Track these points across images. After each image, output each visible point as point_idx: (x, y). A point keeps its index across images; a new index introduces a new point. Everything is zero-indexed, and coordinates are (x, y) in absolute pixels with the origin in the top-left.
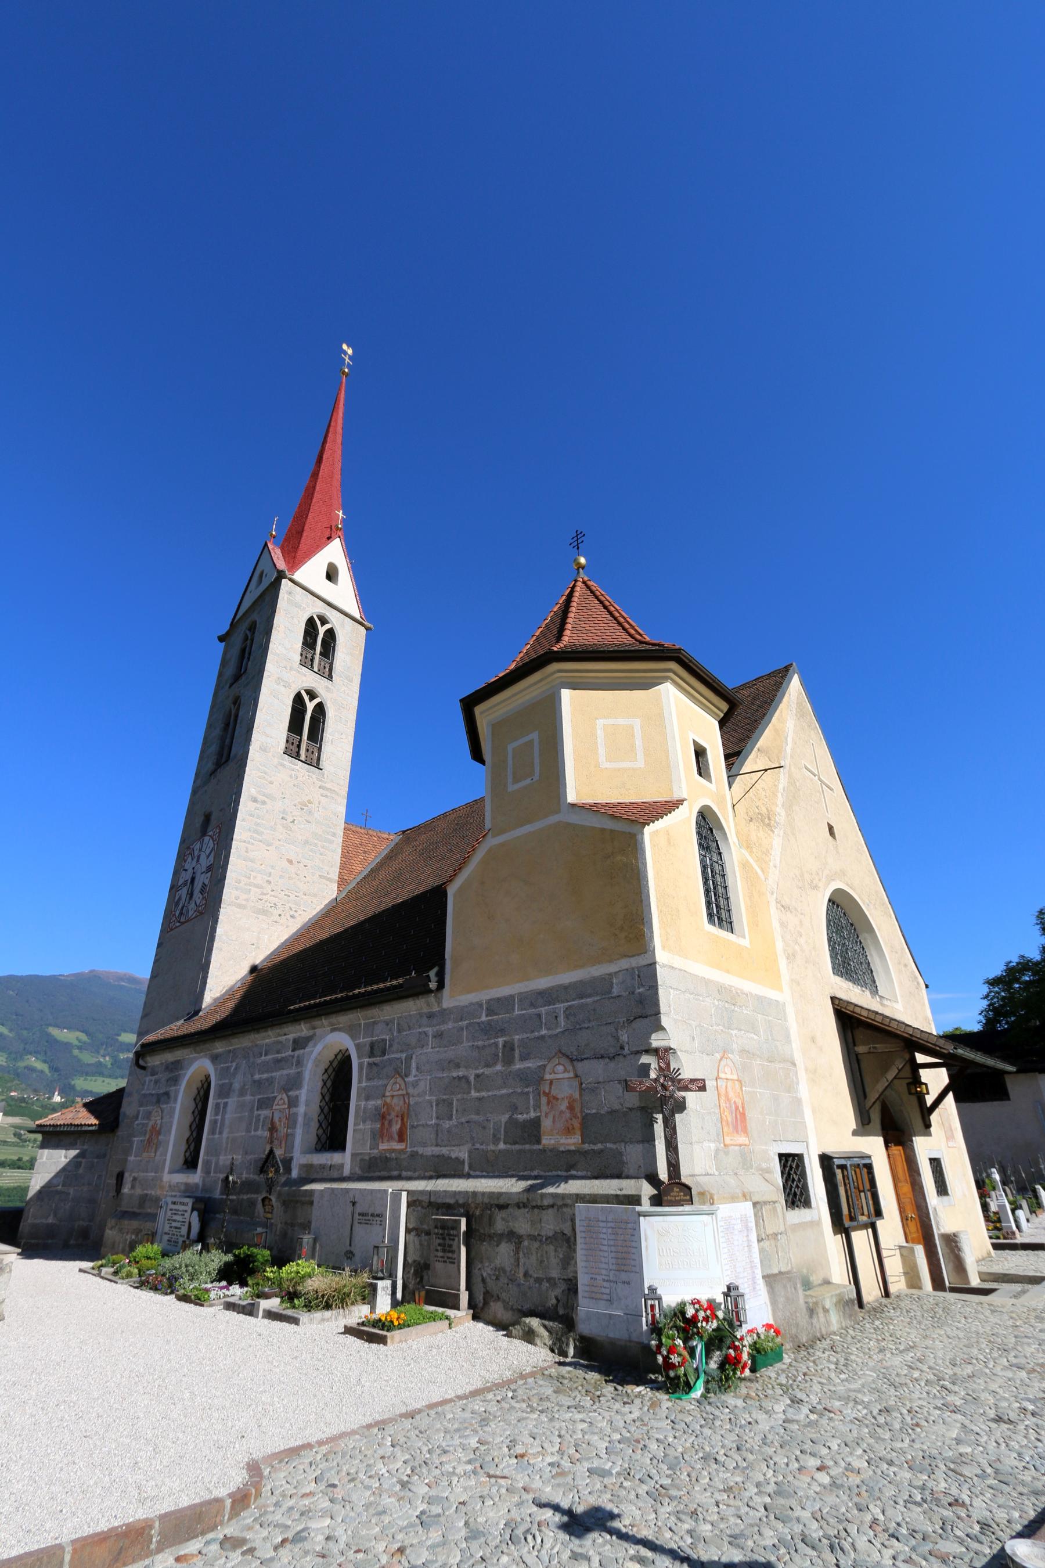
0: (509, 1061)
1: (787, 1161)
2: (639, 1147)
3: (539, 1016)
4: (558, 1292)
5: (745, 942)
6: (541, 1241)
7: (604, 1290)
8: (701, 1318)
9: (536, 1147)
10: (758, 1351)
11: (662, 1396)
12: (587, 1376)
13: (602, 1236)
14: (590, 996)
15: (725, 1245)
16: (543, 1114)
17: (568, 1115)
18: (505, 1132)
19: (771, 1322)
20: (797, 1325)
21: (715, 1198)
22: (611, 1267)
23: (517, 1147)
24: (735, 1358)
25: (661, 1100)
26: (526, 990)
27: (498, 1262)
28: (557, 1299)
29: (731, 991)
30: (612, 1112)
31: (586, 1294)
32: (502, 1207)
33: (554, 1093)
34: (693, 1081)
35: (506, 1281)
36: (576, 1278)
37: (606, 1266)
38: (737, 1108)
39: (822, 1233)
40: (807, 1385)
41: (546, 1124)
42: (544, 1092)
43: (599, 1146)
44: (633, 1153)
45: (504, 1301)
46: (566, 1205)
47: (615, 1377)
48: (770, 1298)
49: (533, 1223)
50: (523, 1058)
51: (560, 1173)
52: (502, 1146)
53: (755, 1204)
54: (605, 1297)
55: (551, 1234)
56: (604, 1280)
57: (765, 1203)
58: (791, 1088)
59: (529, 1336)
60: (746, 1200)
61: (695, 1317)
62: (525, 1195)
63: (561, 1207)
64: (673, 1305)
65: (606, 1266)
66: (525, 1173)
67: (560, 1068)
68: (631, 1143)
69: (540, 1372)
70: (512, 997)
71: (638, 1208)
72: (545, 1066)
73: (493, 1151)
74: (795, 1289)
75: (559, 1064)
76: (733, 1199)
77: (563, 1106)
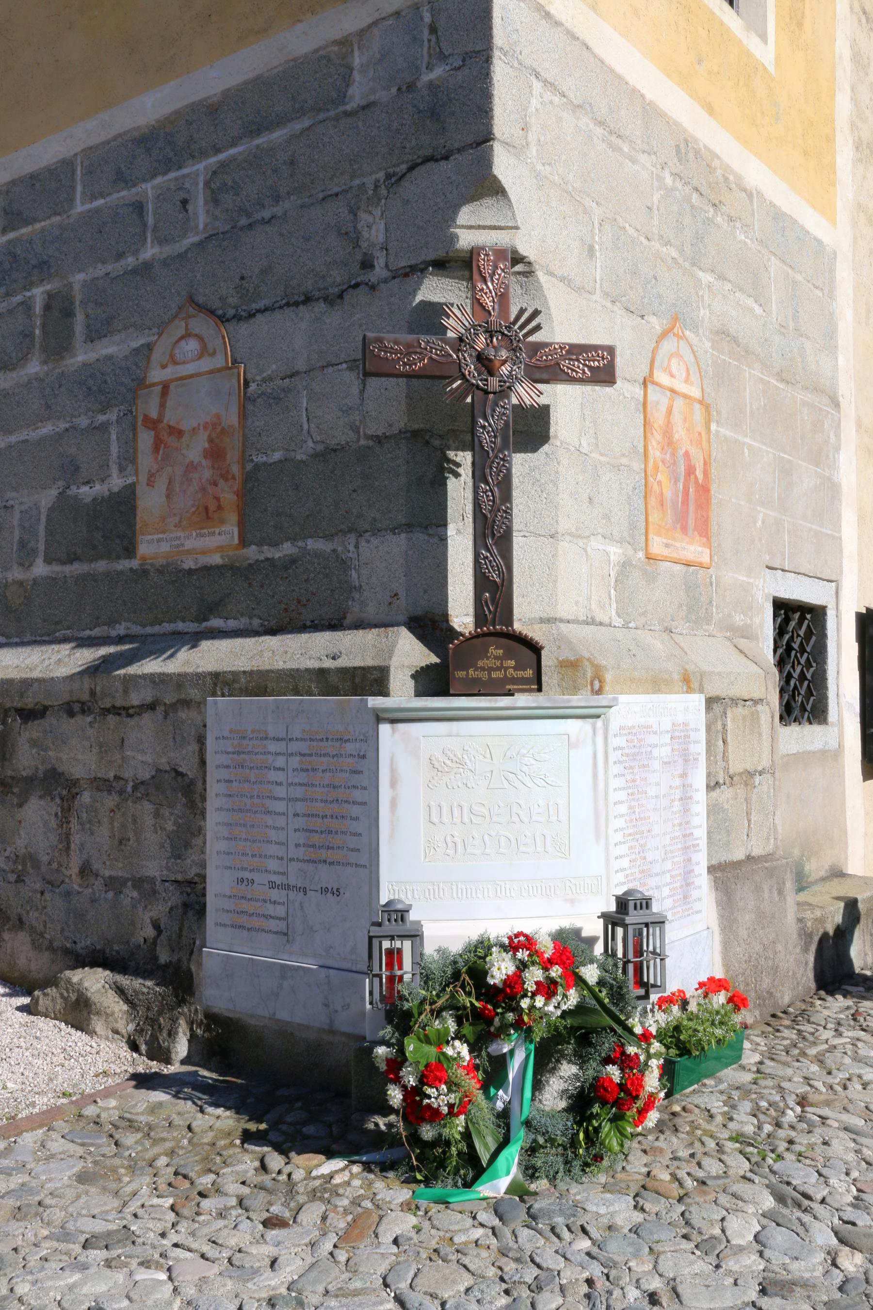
0: (58, 345)
1: (787, 620)
2: (397, 544)
3: (139, 208)
4: (159, 910)
5: (765, 53)
6: (121, 792)
7: (270, 909)
8: (530, 987)
9: (124, 565)
10: (684, 1050)
11: (393, 1192)
12: (200, 1122)
13: (272, 776)
14: (281, 121)
15: (622, 795)
16: (143, 478)
17: (207, 474)
18: (50, 533)
19: (719, 975)
20: (775, 969)
21: (609, 677)
22: (293, 852)
23: (78, 568)
24: (621, 1087)
25: (461, 407)
26: (104, 136)
27: (20, 844)
28: (156, 926)
29: (711, 169)
30: (327, 454)
31: (226, 919)
32: (29, 715)
33: (170, 418)
34: (576, 350)
35: (38, 886)
36: (203, 878)
37: (280, 851)
38: (690, 471)
39: (840, 776)
40: (816, 1139)
41: (150, 502)
42: (146, 418)
43: (287, 549)
44: (379, 560)
45: (32, 929)
46: (186, 703)
47: (274, 1125)
48: (721, 917)
49: (103, 749)
50: (93, 336)
51: (180, 626)
52: (40, 569)
53: (711, 702)
54: (273, 925)
55: (146, 774)
56: (272, 885)
57: (735, 701)
58: (821, 456)
59: (78, 1013)
60: (690, 690)
61: (514, 983)
62: (87, 683)
63: (174, 706)
64: (456, 948)
65: (280, 851)
66: (96, 632)
67: (192, 346)
68: (376, 531)
69: (74, 1114)
70: (67, 164)
71: (374, 702)
72: (149, 347)
73: (21, 584)
74: (780, 892)
75: (187, 335)
76: (657, 684)
77: (194, 450)
